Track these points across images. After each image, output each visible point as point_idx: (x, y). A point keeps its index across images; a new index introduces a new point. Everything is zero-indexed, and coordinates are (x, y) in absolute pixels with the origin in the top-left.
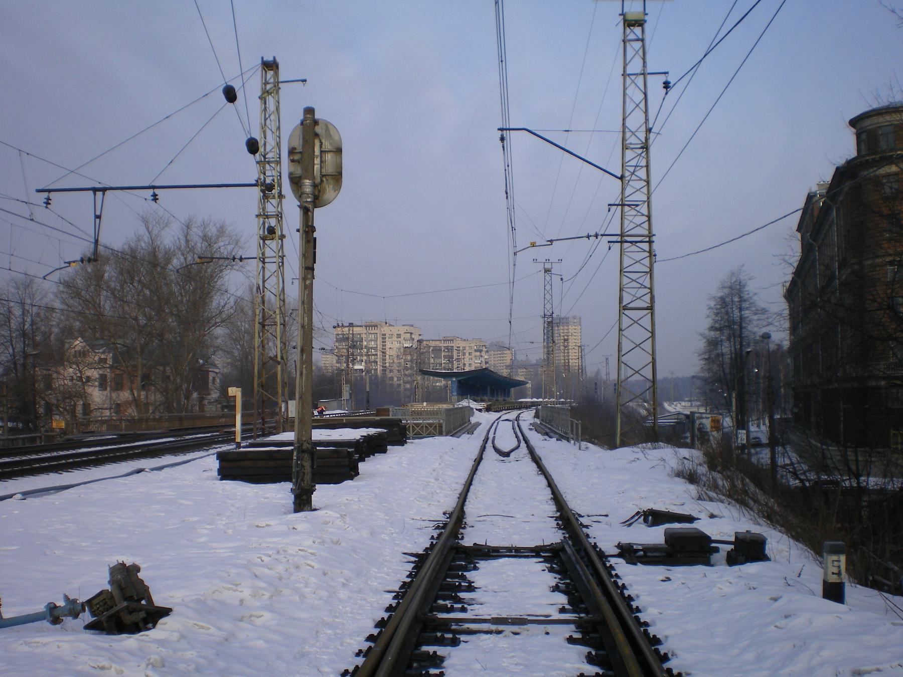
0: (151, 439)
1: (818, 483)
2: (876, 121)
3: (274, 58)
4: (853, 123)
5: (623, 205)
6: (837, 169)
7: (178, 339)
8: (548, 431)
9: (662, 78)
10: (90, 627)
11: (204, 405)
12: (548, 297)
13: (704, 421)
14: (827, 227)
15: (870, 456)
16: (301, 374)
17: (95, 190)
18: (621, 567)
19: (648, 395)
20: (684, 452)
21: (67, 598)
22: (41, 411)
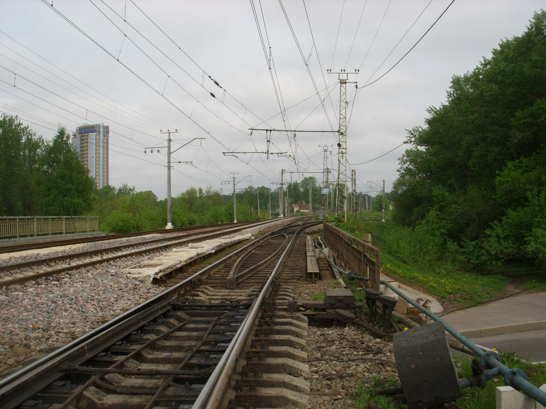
0: (108, 332)
1: (531, 104)
2: (147, 381)
3: (542, 9)
4: (106, 129)
5: (268, 153)
6: (151, 192)
7: (462, 243)
8: (240, 294)
9: (151, 149)
10: (448, 92)
11: (185, 383)
12: (325, 162)
13: (533, 244)
14: (191, 376)
15: (511, 177)
16: (215, 295)
17: (267, 130)
18: (450, 349)
19: (167, 376)
20: (273, 338)
21: (429, 111)
22: (489, 66)
